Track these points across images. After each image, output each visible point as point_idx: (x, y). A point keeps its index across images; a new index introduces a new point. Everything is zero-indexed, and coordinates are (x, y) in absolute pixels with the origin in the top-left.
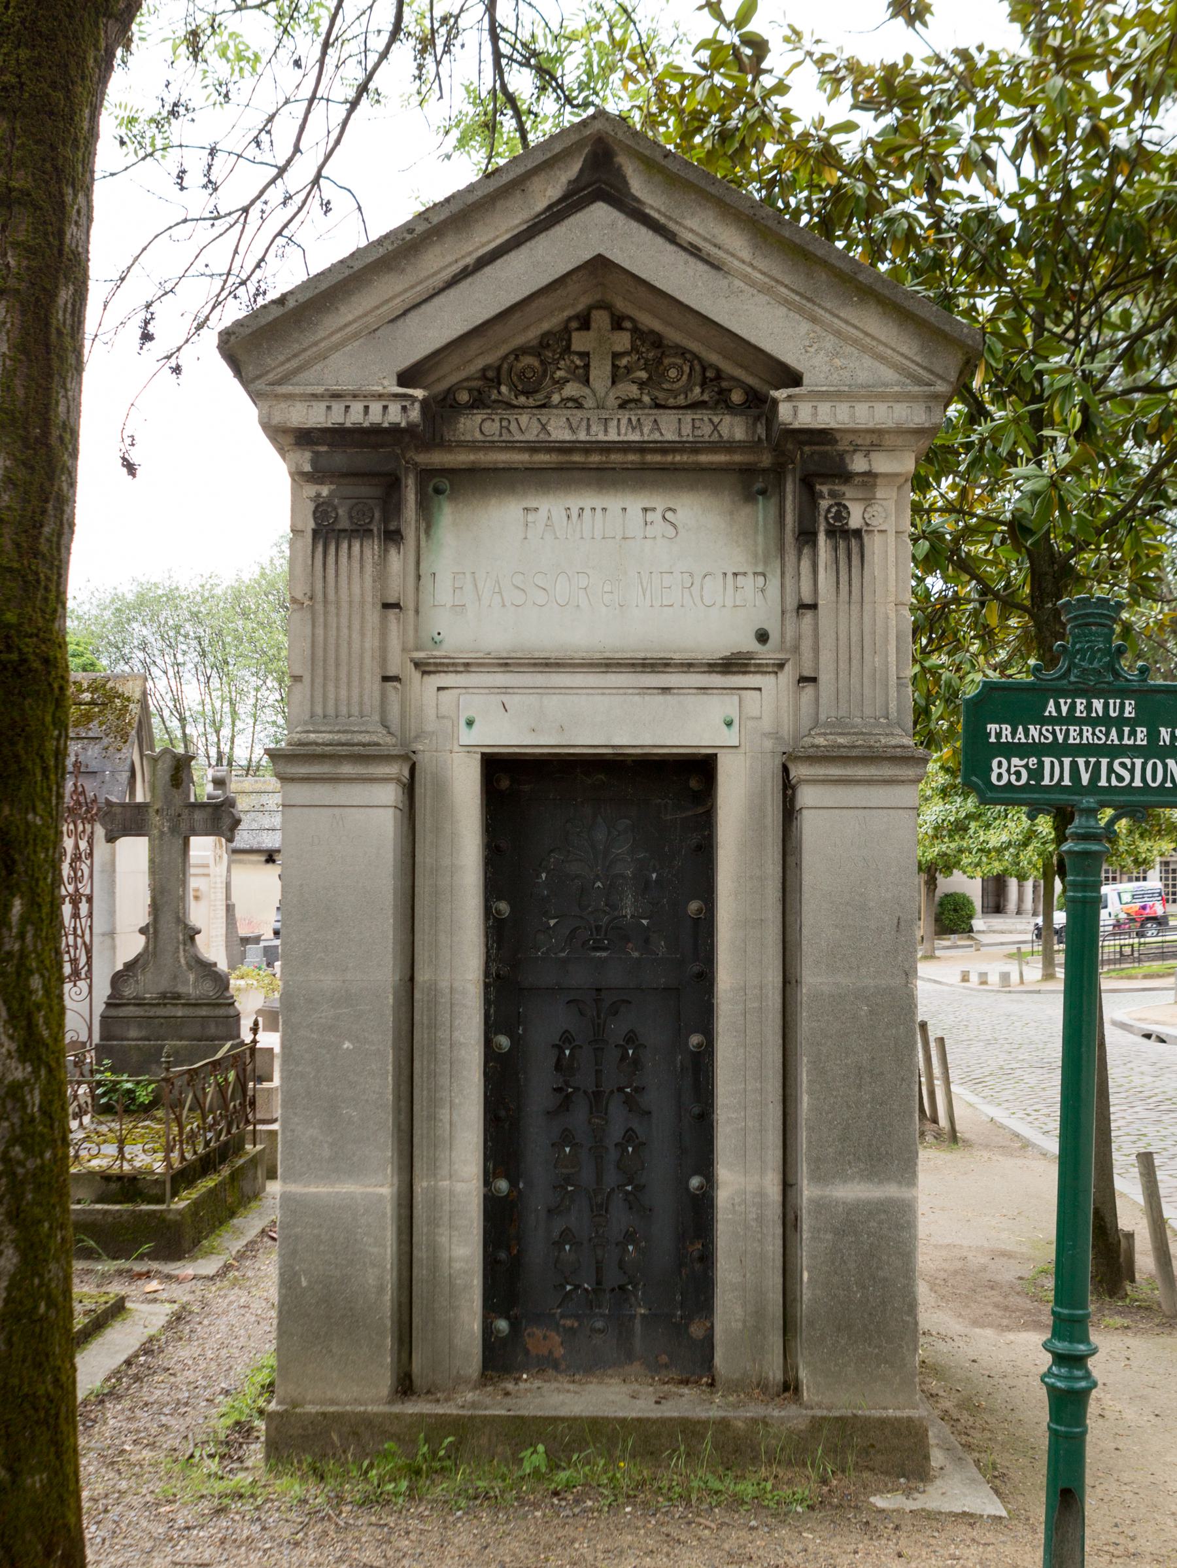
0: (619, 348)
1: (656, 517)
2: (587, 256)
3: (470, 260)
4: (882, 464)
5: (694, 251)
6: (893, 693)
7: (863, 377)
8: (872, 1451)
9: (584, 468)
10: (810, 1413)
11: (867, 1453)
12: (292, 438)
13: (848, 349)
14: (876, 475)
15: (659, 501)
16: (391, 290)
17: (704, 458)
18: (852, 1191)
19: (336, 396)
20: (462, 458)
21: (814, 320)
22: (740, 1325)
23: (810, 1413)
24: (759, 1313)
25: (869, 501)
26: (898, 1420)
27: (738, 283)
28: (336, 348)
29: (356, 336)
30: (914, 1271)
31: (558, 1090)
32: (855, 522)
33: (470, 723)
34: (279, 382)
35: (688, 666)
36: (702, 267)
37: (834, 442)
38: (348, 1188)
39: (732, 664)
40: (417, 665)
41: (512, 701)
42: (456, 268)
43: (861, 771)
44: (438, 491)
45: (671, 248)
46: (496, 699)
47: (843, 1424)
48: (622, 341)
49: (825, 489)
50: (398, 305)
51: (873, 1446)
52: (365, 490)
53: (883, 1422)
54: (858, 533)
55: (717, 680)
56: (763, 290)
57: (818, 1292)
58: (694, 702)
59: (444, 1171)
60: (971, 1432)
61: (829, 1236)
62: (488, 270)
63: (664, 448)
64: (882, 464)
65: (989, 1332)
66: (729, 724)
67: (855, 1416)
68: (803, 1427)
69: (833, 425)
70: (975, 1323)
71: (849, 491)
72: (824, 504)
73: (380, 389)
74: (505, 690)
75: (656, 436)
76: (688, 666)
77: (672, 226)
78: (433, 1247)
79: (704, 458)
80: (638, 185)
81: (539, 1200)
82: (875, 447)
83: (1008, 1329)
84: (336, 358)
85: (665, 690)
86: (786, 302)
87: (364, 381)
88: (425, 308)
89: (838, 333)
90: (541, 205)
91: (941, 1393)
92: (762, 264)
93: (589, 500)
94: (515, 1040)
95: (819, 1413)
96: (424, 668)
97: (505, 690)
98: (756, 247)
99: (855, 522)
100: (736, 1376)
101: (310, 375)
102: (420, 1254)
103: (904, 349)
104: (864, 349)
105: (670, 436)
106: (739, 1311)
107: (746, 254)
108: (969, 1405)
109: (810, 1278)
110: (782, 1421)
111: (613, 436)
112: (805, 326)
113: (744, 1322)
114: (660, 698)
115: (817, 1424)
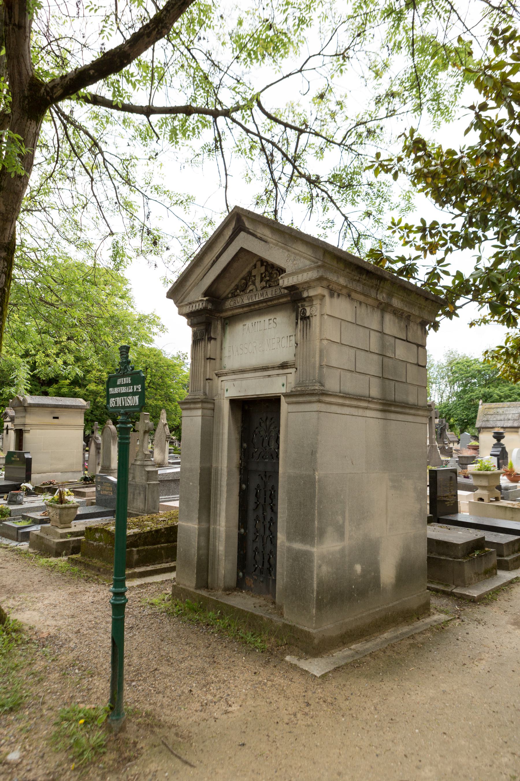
0: (262, 272)
1: (271, 321)
2: (239, 248)
3: (214, 258)
4: (312, 293)
5: (261, 239)
6: (317, 371)
7: (301, 265)
9: (256, 310)
12: (188, 315)
13: (298, 257)
14: (311, 297)
15: (272, 317)
16: (199, 271)
17: (281, 300)
18: (297, 546)
19: (190, 303)
20: (229, 313)
21: (288, 251)
25: (311, 306)
26: (306, 631)
27: (271, 245)
28: (190, 291)
29: (194, 286)
31: (256, 503)
32: (308, 314)
33: (227, 390)
34: (181, 302)
35: (273, 368)
36: (263, 243)
37: (298, 289)
38: (190, 524)
39: (284, 366)
40: (216, 375)
41: (236, 383)
42: (212, 261)
43: (301, 399)
44: (227, 324)
45: (256, 239)
46: (232, 383)
47: (292, 629)
48: (263, 269)
49: (300, 304)
50: (201, 275)
52: (202, 327)
53: (302, 631)
54: (308, 317)
55: (281, 371)
56: (277, 245)
58: (274, 379)
59: (218, 523)
61: (291, 561)
62: (219, 260)
63: (271, 300)
64: (312, 293)
66: (283, 385)
67: (271, 621)
69: (293, 284)
71: (306, 304)
72: (300, 309)
73: (197, 300)
74: (235, 380)
75: (267, 297)
76: (273, 368)
77: (255, 233)
78: (214, 546)
79: (281, 300)
80: (247, 224)
81: (251, 537)
82: (309, 287)
84: (191, 293)
85: (269, 376)
86: (282, 247)
87: (197, 297)
88: (208, 274)
89: (294, 253)
90: (227, 237)
92: (274, 237)
93: (257, 320)
94: (247, 486)
96: (218, 375)
97: (235, 380)
98: (272, 233)
99: (308, 314)
101: (186, 299)
102: (211, 547)
103: (309, 253)
104: (301, 256)
105: (270, 296)
107: (270, 236)
111: (257, 299)
112: (287, 253)
114: (267, 379)
115: (285, 626)
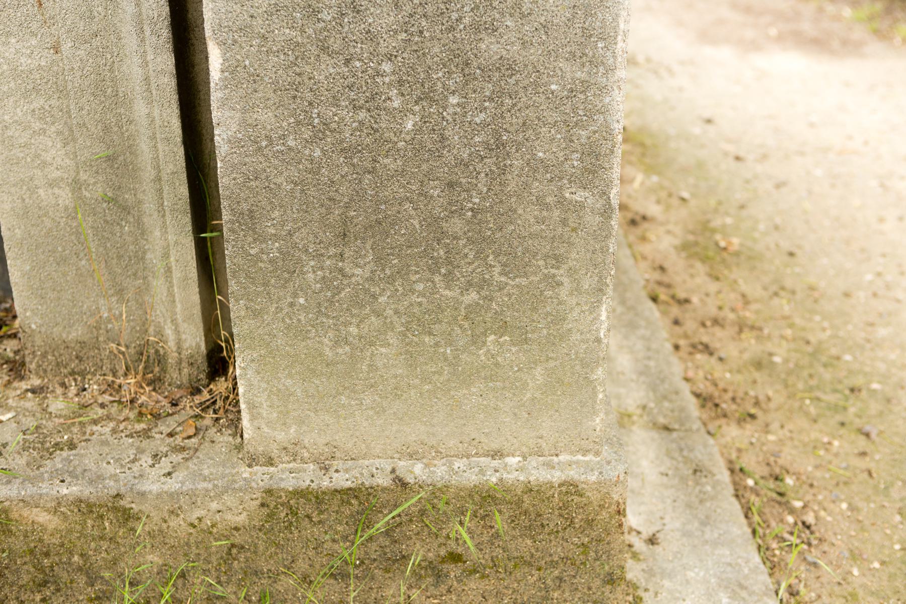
8: (454, 571)
10: (260, 476)
11: (439, 577)
22: (65, 196)
23: (260, 476)
24: (118, 162)
30: (608, 37)
51: (455, 558)
57: (266, 117)
60: (717, 337)
65: (725, 53)
68: (241, 519)
70: (705, 37)
83: (754, 46)
91: (653, 209)
95: (291, 477)
100: (77, 333)
106: (56, 154)
108: (706, 248)
109: (230, 69)
110: (174, 505)
113: (77, 186)
115: (284, 511)
